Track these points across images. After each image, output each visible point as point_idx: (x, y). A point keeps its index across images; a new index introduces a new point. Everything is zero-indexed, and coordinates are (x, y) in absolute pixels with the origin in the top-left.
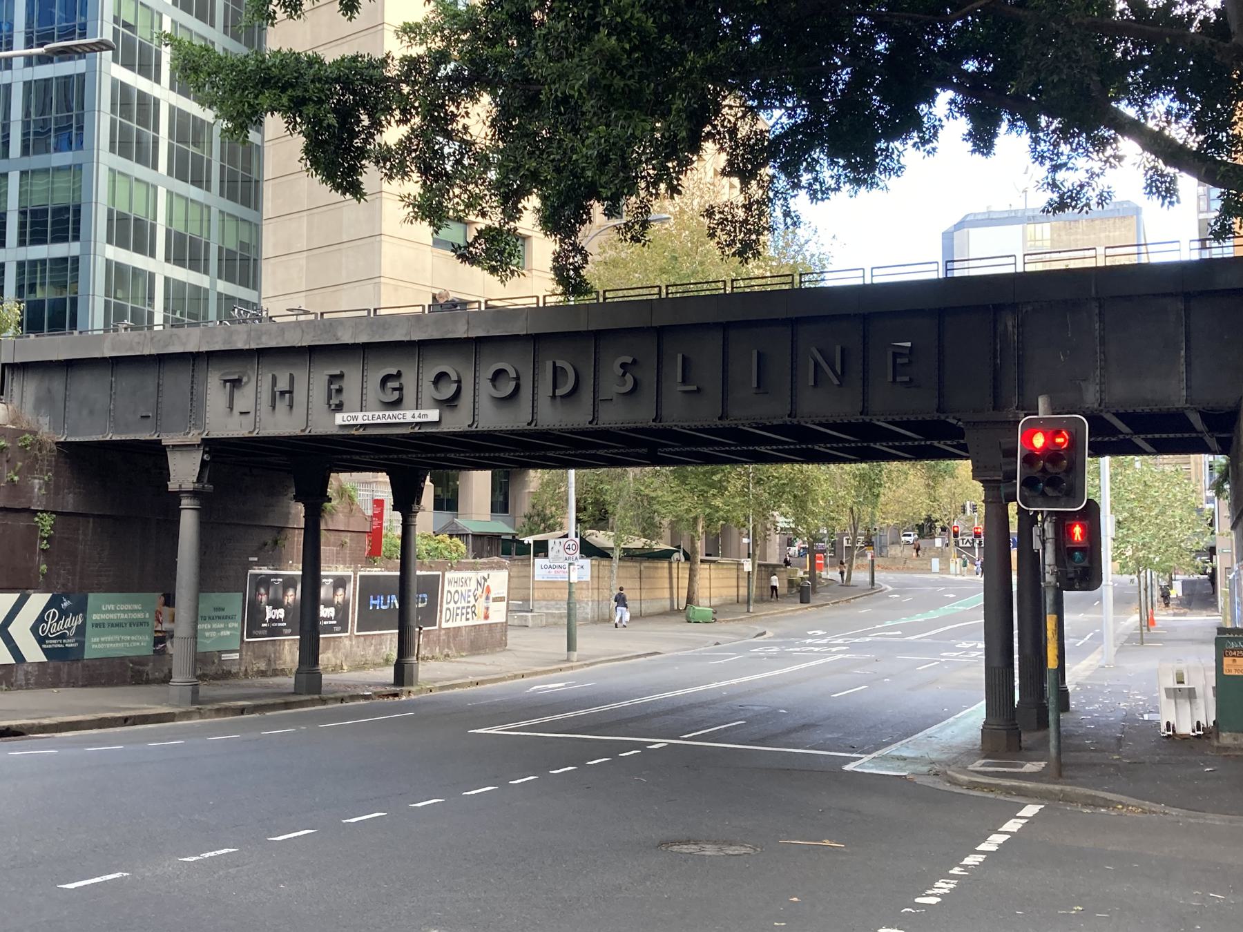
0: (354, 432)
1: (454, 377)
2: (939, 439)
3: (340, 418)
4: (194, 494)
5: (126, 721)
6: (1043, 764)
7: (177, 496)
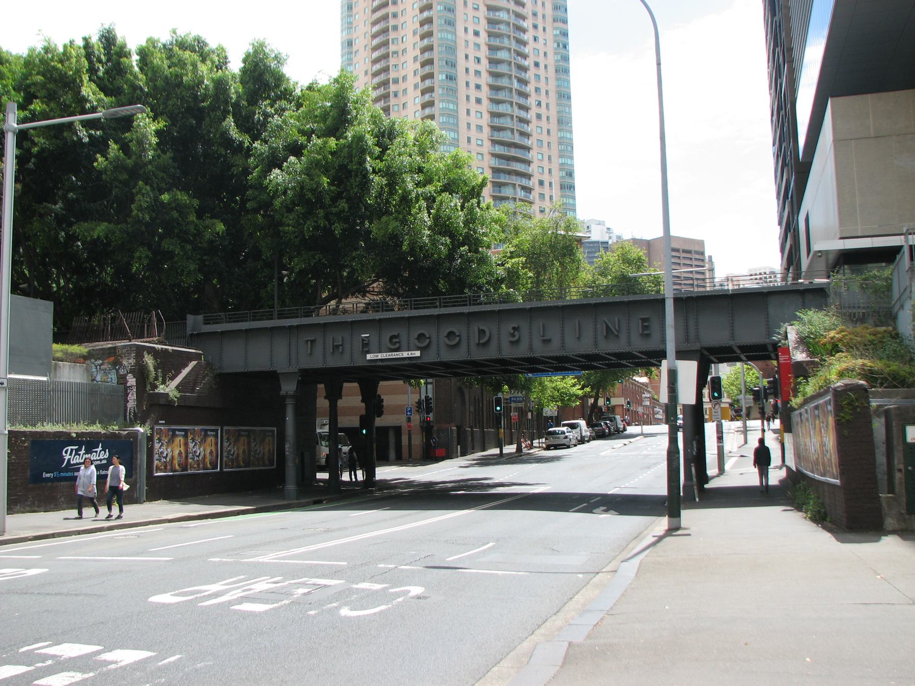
0: (380, 363)
1: (457, 334)
2: (594, 361)
3: (369, 357)
4: (292, 397)
5: (53, 536)
6: (151, 599)
7: (284, 398)
